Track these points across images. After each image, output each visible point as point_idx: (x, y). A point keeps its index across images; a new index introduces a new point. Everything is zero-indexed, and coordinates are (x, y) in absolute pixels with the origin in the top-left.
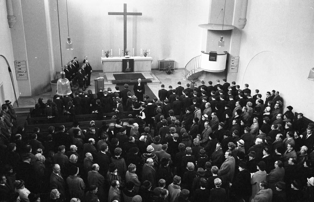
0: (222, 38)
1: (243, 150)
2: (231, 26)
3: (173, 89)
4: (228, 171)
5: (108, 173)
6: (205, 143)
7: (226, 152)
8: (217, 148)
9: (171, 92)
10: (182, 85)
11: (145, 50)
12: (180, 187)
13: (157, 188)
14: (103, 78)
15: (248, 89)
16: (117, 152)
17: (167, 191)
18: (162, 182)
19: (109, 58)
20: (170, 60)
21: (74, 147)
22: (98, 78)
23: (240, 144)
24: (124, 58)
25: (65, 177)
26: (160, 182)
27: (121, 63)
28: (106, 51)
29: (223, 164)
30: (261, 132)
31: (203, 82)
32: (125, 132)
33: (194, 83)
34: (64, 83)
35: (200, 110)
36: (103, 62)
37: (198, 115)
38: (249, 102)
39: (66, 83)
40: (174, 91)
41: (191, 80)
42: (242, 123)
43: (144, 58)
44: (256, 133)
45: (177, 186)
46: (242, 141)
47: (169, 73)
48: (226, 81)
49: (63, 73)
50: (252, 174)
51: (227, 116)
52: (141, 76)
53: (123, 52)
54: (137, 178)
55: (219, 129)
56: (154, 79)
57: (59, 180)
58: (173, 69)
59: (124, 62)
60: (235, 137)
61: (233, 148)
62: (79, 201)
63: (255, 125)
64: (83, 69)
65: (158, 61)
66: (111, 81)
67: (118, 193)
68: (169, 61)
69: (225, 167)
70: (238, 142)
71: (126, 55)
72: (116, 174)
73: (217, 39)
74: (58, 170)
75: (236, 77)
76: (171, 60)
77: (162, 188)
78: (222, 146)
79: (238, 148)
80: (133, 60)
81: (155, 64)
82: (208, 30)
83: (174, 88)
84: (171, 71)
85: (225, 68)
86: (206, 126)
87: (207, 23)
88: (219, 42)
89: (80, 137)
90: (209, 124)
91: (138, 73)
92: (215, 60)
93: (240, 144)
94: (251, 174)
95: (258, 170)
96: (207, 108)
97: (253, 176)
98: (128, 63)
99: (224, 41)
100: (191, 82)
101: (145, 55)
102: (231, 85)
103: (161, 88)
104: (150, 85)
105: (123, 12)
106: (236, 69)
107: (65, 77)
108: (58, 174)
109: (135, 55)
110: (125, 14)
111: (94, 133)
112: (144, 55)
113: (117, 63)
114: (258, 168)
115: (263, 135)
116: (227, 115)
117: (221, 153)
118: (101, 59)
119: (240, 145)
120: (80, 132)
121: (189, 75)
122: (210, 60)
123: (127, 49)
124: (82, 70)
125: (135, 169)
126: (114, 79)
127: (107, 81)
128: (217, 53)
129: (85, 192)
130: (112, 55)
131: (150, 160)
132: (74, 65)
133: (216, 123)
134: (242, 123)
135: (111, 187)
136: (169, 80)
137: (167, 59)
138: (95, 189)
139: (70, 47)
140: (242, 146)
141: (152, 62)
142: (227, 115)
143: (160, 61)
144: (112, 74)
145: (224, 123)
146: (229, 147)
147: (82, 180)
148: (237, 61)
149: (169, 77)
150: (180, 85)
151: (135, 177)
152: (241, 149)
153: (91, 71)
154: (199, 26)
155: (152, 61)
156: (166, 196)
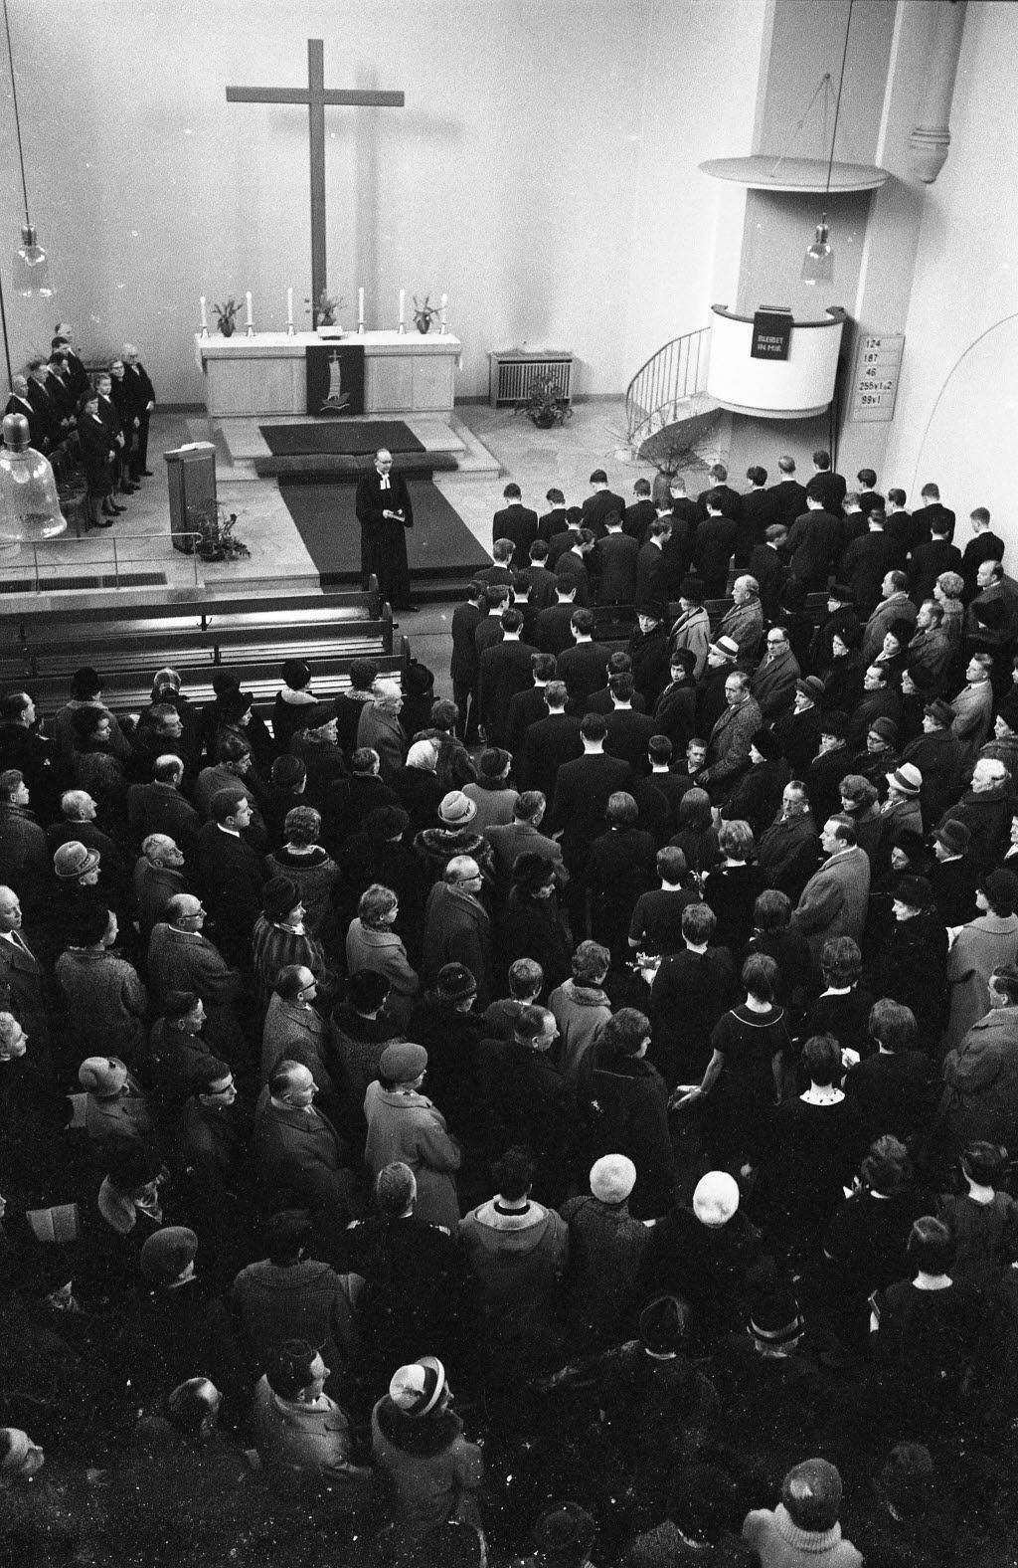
0: (823, 238)
1: (914, 817)
2: (873, 169)
3: (567, 506)
4: (836, 916)
5: (261, 925)
6: (725, 778)
7: (829, 822)
8: (786, 805)
9: (557, 520)
10: (613, 487)
11: (421, 299)
12: (604, 995)
13: (501, 1002)
14: (210, 445)
15: (940, 505)
16: (305, 828)
17: (549, 1020)
18: (522, 975)
19: (237, 341)
20: (548, 353)
21: (79, 799)
22: (186, 447)
23: (901, 788)
24: (314, 339)
25: (48, 954)
26: (513, 975)
27: (299, 367)
28: (222, 301)
29: (811, 883)
30: (1006, 727)
31: (720, 472)
32: (331, 730)
33: (671, 475)
34: (27, 474)
35: (703, 617)
36: (204, 361)
37: (693, 639)
38: (951, 574)
39: (36, 475)
40: (574, 514)
41: (659, 462)
42: (907, 686)
43: (415, 338)
44: (978, 732)
45: (591, 992)
46: (911, 772)
47: (546, 422)
48: (723, 479)
49: (17, 421)
50: (952, 932)
51: (838, 647)
52: (398, 436)
53: (309, 306)
54: (400, 956)
55: (797, 711)
56: (467, 453)
57: (16, 965)
58: (567, 401)
59: (316, 359)
60: (877, 755)
61: (864, 803)
62: (118, 1068)
63: (975, 694)
64: (107, 397)
65: (489, 356)
66: (248, 462)
67: (308, 1027)
68: (547, 358)
69: (816, 895)
70: (890, 777)
71: (322, 324)
72: (299, 929)
73: (795, 238)
74: (13, 915)
75: (884, 445)
76: (555, 353)
77: (526, 1003)
78: (810, 796)
79: (887, 805)
80: (361, 348)
81: (475, 371)
82: (749, 189)
83: (574, 500)
84: (558, 412)
85: (829, 397)
86: (733, 695)
87: (746, 151)
88: (807, 256)
89: (103, 746)
90: (746, 683)
91: (387, 419)
92: (783, 355)
93: (901, 788)
94: (948, 929)
95: (983, 913)
96: (744, 604)
97: (959, 942)
98: (335, 368)
99: (831, 254)
100: (659, 467)
101: (424, 326)
102: (854, 486)
103: (504, 504)
104: (448, 487)
105: (305, 86)
106: (887, 398)
107: (30, 445)
108: (8, 937)
109: (372, 325)
110: (316, 96)
111: (177, 731)
112: (414, 325)
113: (279, 369)
114: (981, 901)
115: (1011, 744)
116: (836, 639)
117: (807, 828)
118: (193, 342)
119: (900, 792)
120: (105, 722)
121: (644, 431)
122: (756, 353)
123: (331, 293)
124: (102, 401)
125: (393, 914)
126: (264, 450)
127: (229, 461)
128: (791, 318)
129: (148, 1021)
130: (250, 323)
131: (464, 865)
132: (59, 378)
133: (785, 683)
134: (907, 686)
135: (276, 999)
136: (547, 456)
137: (535, 348)
138: (187, 1007)
139: (34, 278)
140: (910, 794)
141: (457, 362)
142: (836, 639)
143: (498, 355)
144: (257, 423)
145: (822, 680)
146: (844, 800)
147: (131, 969)
148: (893, 358)
149: (542, 439)
150: (601, 487)
151: (394, 951)
152: (905, 810)
153: (150, 405)
154: (705, 166)
155: (457, 356)
156: (536, 1043)
